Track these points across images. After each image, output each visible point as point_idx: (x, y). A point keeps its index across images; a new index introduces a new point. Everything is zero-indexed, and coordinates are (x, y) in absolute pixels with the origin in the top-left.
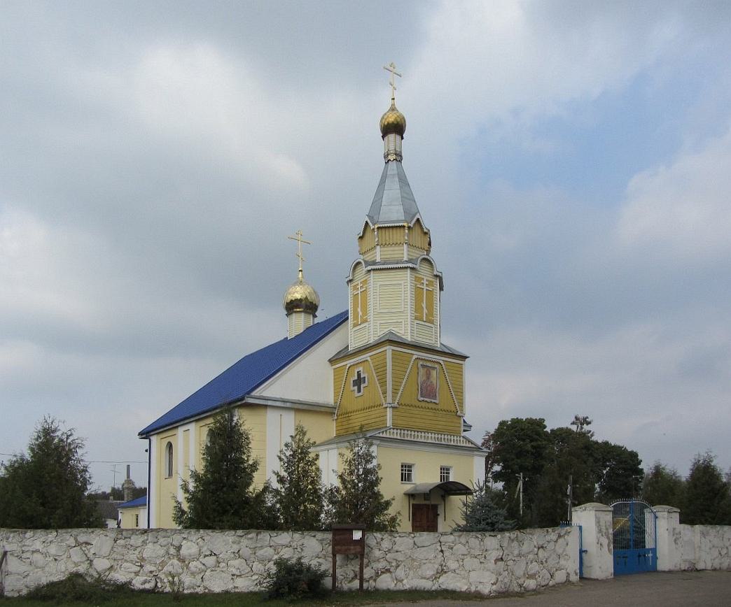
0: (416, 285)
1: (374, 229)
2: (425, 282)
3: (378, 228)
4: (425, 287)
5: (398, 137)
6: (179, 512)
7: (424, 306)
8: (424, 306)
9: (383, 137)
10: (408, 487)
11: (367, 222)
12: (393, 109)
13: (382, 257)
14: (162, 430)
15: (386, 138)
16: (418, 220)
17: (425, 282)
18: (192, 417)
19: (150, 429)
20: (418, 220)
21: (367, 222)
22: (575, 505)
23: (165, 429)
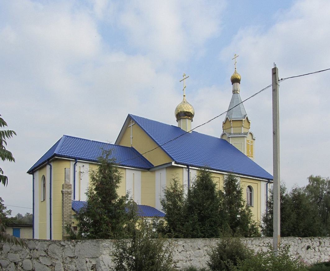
0: (247, 143)
1: (231, 121)
2: (250, 142)
3: (232, 121)
4: (250, 144)
5: (238, 84)
6: (172, 188)
7: (250, 151)
8: (250, 151)
9: (232, 84)
10: (74, 261)
11: (227, 118)
12: (235, 72)
13: (234, 132)
14: (252, 178)
15: (233, 84)
16: (247, 117)
17: (250, 142)
18: (89, 160)
19: (36, 166)
20: (247, 117)
21: (227, 118)
22: (323, 182)
23: (257, 179)
